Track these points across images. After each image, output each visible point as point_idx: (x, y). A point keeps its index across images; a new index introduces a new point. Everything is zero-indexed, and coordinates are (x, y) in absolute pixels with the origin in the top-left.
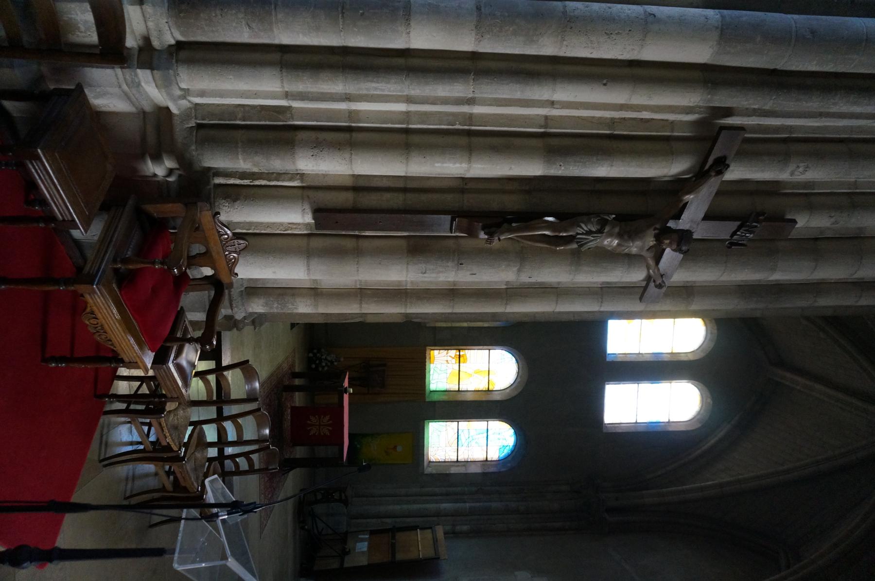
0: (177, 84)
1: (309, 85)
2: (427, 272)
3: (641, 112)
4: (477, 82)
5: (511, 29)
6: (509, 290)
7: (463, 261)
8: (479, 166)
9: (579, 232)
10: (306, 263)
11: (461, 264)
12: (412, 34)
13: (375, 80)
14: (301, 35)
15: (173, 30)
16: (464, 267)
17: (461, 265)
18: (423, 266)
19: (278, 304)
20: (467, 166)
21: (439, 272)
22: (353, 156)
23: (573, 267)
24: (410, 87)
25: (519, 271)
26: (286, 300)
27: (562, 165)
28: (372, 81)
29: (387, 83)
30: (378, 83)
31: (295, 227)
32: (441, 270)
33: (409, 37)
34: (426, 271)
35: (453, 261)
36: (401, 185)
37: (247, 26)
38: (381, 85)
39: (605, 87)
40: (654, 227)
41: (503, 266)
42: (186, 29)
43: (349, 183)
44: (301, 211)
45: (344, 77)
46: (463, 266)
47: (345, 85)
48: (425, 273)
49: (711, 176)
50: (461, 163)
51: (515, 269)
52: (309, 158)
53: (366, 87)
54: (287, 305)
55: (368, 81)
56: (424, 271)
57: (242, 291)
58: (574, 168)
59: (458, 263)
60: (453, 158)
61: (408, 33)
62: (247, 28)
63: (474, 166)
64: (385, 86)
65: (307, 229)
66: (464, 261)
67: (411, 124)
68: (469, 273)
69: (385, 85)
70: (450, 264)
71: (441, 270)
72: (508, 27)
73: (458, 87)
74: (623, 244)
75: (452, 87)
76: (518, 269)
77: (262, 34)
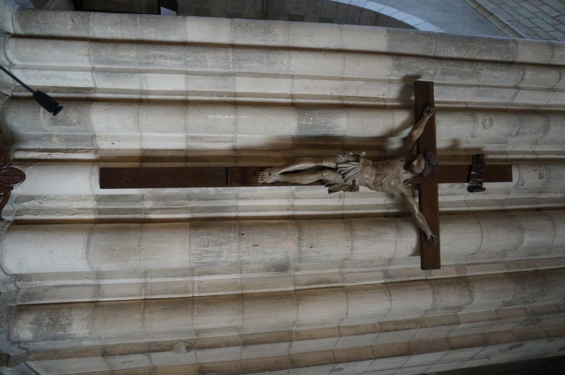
0: (5, 49)
1: (109, 53)
2: (210, 244)
3: (357, 81)
4: (235, 52)
5: (254, 25)
6: (297, 292)
7: (244, 232)
8: (244, 117)
9: (338, 162)
10: (86, 239)
11: (242, 235)
12: (187, 26)
13: (160, 49)
14: (109, 28)
15: (15, 22)
16: (246, 237)
17: (243, 236)
18: (205, 237)
19: (50, 319)
20: (234, 117)
21: (221, 244)
22: (140, 110)
23: (348, 233)
24: (186, 54)
25: (299, 239)
26: (60, 314)
27: (310, 116)
28: (157, 50)
29: (169, 51)
30: (162, 51)
31: (84, 211)
32: (223, 241)
33: (186, 29)
34: (208, 244)
35: (235, 232)
36: (183, 154)
37: (71, 20)
38: (164, 52)
39: (325, 55)
40: (400, 159)
41: (283, 235)
42: (25, 22)
43: (138, 154)
44: (89, 173)
45: (137, 47)
46: (245, 236)
47: (138, 52)
48: (208, 246)
49: (425, 116)
50: (229, 115)
51: (295, 237)
52: (102, 111)
53: (153, 54)
54: (60, 320)
55: (155, 50)
56: (206, 245)
57: (13, 307)
58: (320, 119)
59: (240, 234)
60: (223, 111)
61: (185, 26)
62: (71, 22)
63: (240, 117)
64: (167, 54)
65: (95, 213)
66: (245, 232)
67: (190, 96)
68: (251, 244)
69: (167, 53)
70: (232, 235)
71: (223, 241)
72: (251, 24)
73: (221, 55)
74: (380, 173)
75: (217, 55)
76: (298, 237)
77: (81, 26)
